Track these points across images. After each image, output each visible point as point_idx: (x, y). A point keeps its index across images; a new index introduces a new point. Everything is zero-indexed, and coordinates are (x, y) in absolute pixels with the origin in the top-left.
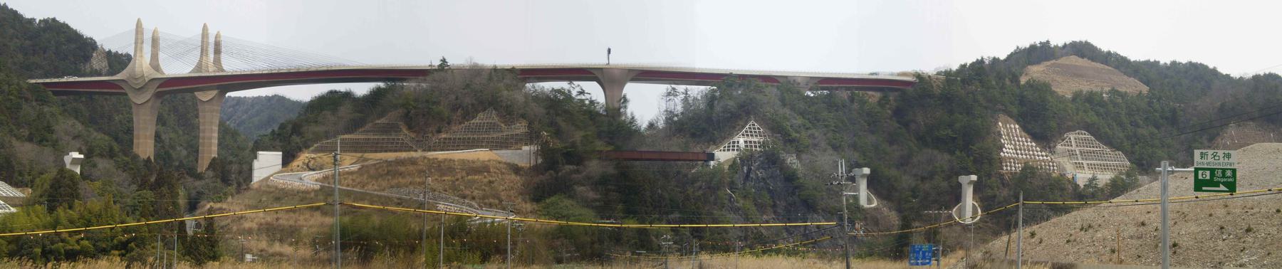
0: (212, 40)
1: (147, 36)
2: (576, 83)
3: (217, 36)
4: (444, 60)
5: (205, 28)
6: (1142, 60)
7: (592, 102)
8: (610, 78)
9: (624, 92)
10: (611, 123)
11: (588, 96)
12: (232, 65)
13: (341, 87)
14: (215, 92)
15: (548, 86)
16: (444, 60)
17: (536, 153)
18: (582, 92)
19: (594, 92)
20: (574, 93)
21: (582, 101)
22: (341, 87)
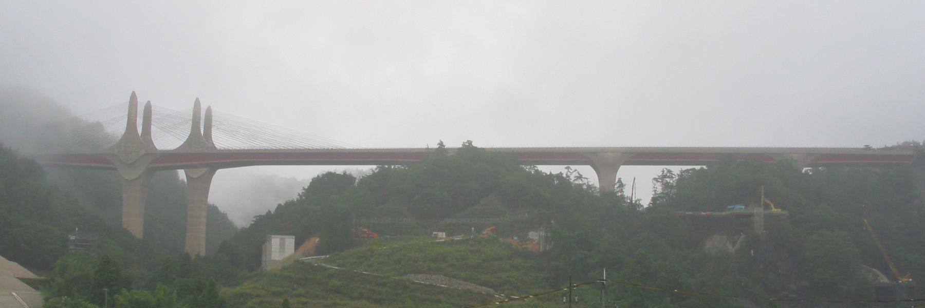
0: (141, 109)
1: (141, 109)
2: (573, 167)
3: (209, 112)
4: (441, 144)
5: (133, 97)
6: (895, 144)
7: (589, 187)
8: (605, 160)
9: (618, 176)
10: (611, 204)
11: (585, 181)
12: (222, 141)
13: (339, 169)
14: (205, 170)
15: (545, 169)
16: (441, 144)
17: (198, 256)
18: (580, 177)
19: (588, 175)
20: (572, 178)
21: (580, 186)
22: (339, 169)
